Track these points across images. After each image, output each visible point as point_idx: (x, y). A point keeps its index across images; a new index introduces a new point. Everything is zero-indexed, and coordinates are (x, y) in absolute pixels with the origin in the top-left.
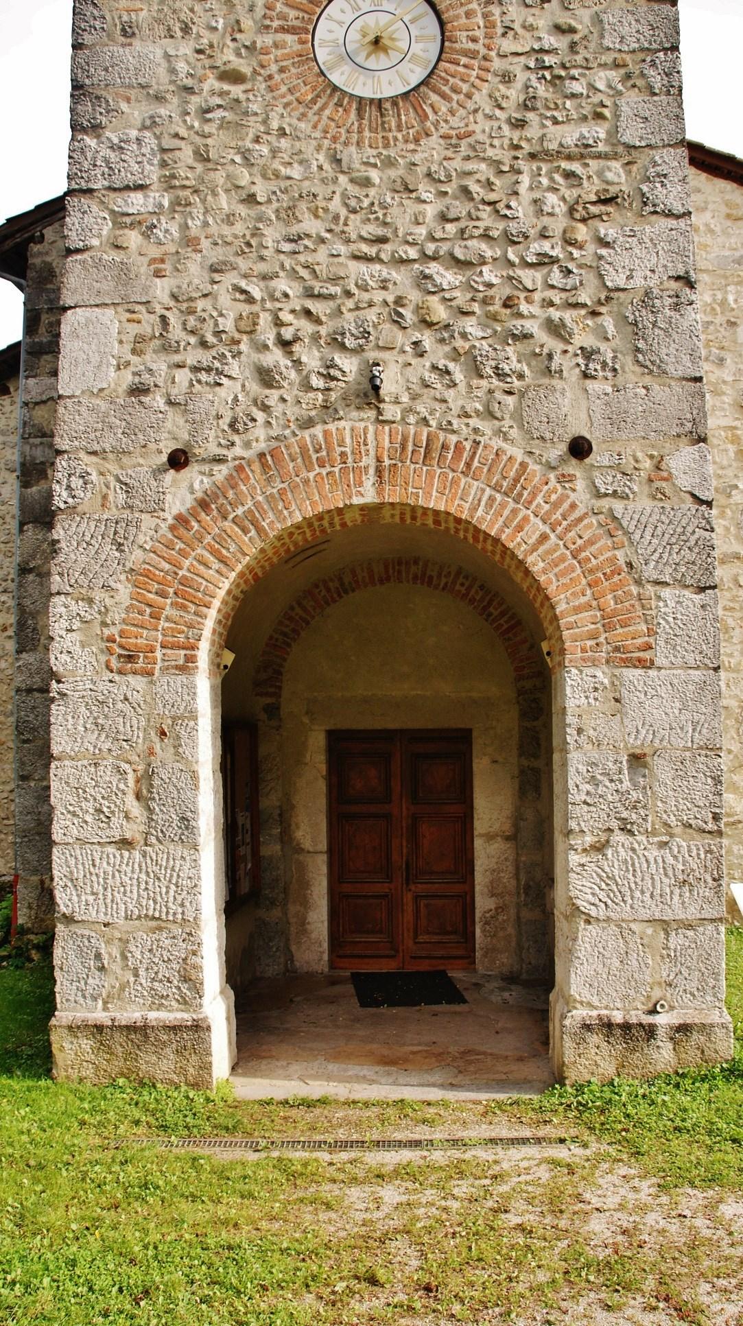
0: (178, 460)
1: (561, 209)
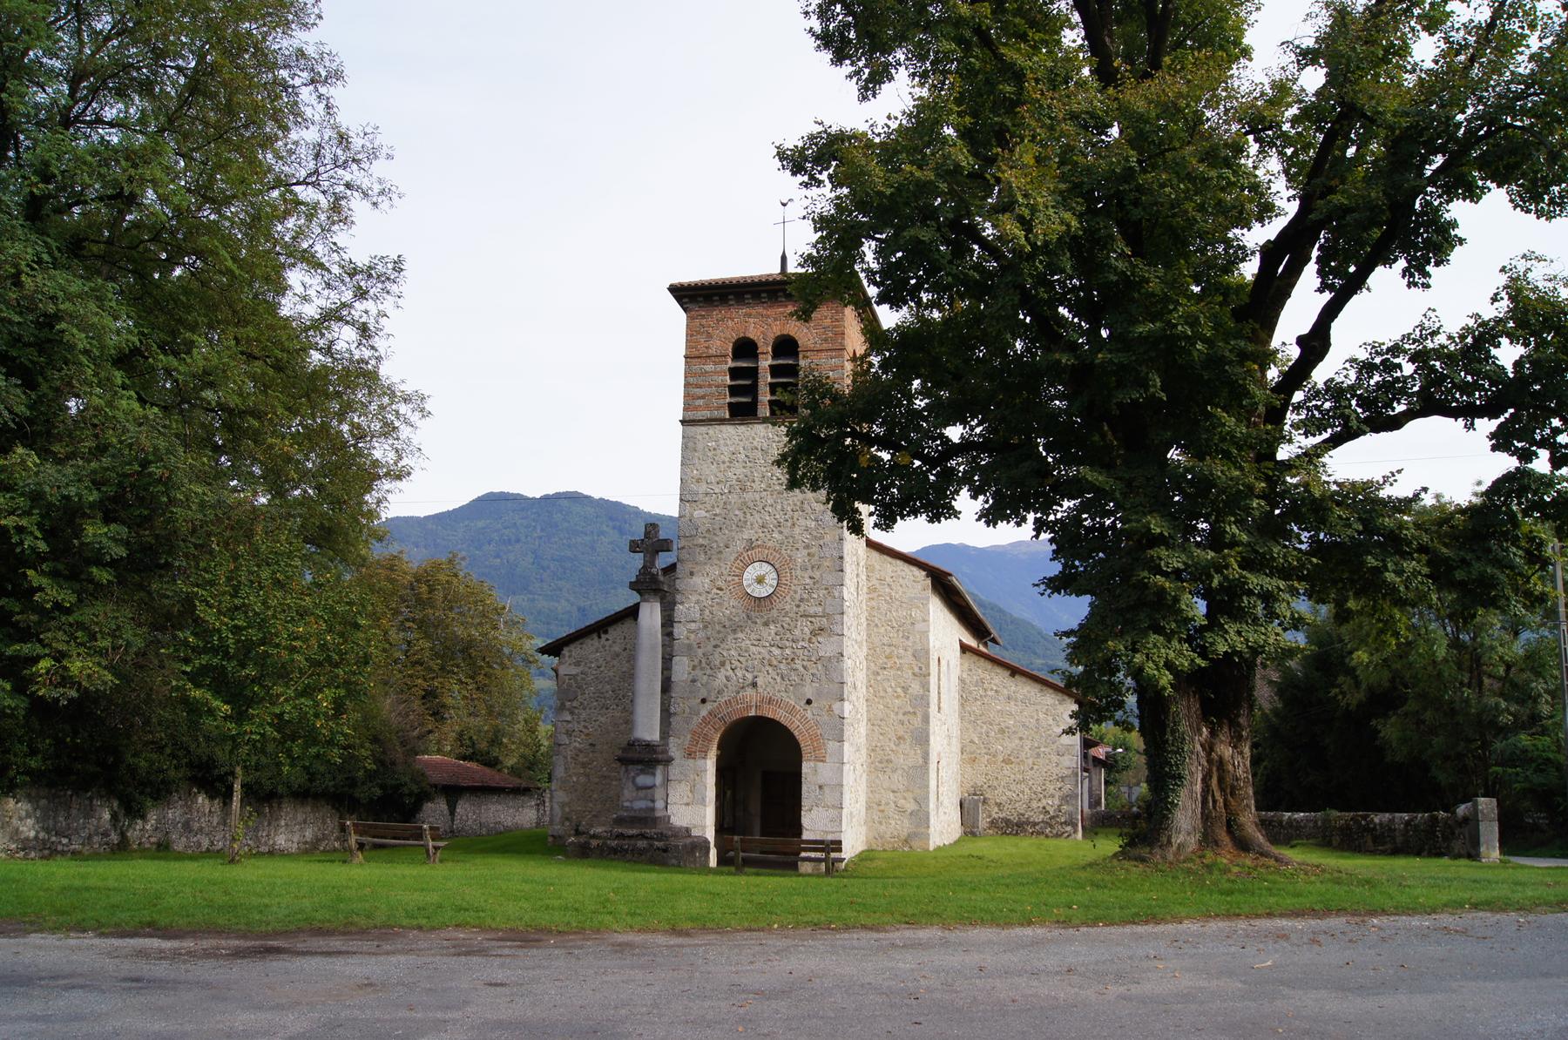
0: (704, 701)
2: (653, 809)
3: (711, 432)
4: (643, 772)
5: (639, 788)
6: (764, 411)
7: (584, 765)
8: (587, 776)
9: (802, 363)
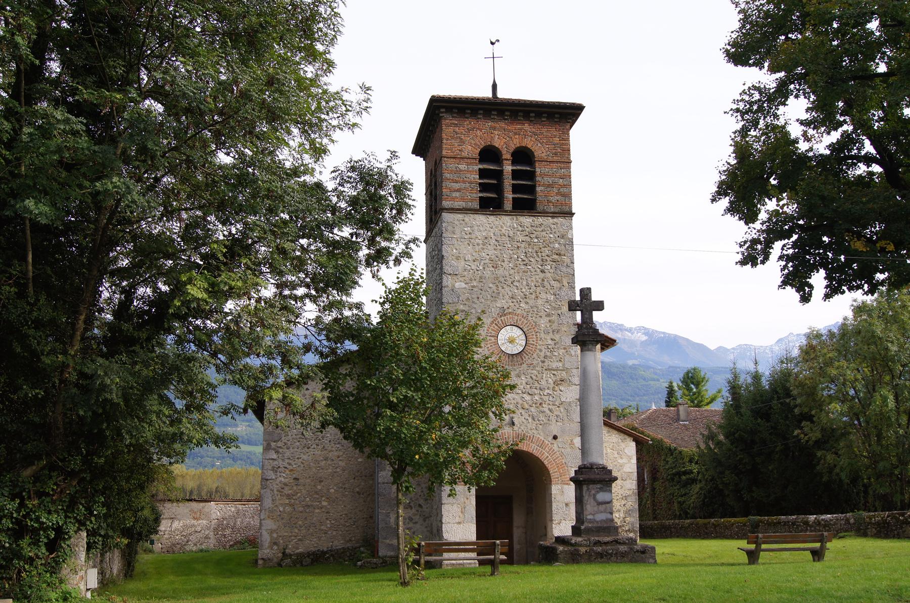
1: (552, 382)
2: (612, 520)
3: (467, 219)
4: (601, 490)
5: (600, 504)
6: (508, 205)
7: (289, 496)
8: (292, 505)
9: (538, 170)
